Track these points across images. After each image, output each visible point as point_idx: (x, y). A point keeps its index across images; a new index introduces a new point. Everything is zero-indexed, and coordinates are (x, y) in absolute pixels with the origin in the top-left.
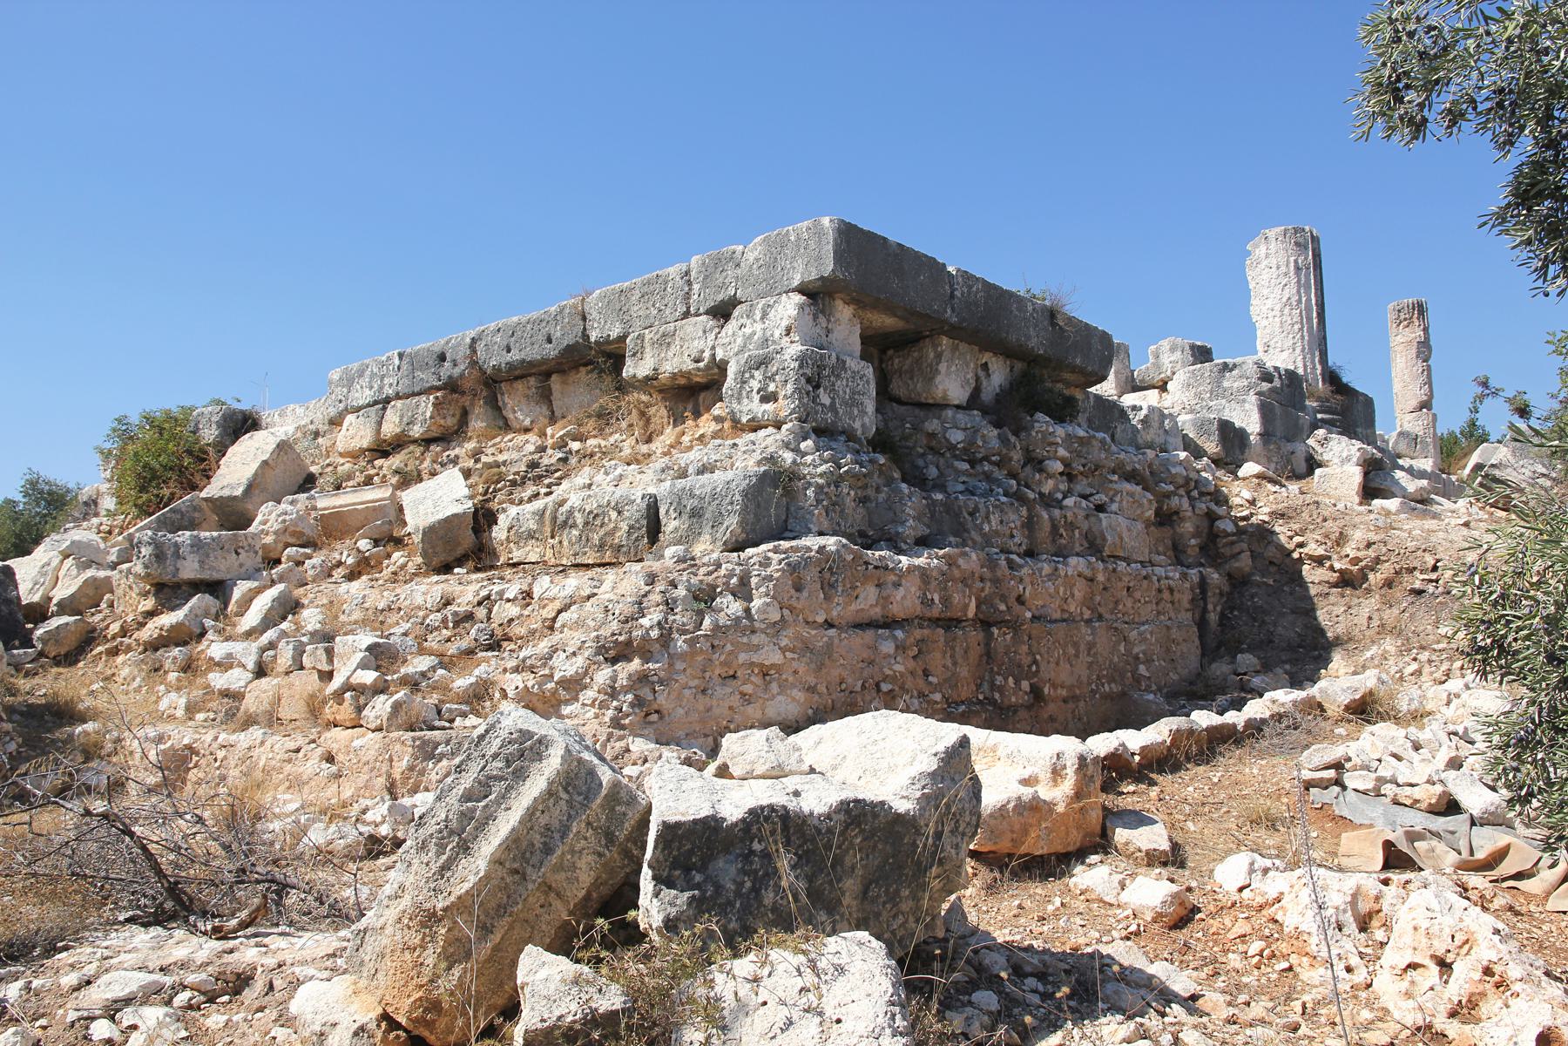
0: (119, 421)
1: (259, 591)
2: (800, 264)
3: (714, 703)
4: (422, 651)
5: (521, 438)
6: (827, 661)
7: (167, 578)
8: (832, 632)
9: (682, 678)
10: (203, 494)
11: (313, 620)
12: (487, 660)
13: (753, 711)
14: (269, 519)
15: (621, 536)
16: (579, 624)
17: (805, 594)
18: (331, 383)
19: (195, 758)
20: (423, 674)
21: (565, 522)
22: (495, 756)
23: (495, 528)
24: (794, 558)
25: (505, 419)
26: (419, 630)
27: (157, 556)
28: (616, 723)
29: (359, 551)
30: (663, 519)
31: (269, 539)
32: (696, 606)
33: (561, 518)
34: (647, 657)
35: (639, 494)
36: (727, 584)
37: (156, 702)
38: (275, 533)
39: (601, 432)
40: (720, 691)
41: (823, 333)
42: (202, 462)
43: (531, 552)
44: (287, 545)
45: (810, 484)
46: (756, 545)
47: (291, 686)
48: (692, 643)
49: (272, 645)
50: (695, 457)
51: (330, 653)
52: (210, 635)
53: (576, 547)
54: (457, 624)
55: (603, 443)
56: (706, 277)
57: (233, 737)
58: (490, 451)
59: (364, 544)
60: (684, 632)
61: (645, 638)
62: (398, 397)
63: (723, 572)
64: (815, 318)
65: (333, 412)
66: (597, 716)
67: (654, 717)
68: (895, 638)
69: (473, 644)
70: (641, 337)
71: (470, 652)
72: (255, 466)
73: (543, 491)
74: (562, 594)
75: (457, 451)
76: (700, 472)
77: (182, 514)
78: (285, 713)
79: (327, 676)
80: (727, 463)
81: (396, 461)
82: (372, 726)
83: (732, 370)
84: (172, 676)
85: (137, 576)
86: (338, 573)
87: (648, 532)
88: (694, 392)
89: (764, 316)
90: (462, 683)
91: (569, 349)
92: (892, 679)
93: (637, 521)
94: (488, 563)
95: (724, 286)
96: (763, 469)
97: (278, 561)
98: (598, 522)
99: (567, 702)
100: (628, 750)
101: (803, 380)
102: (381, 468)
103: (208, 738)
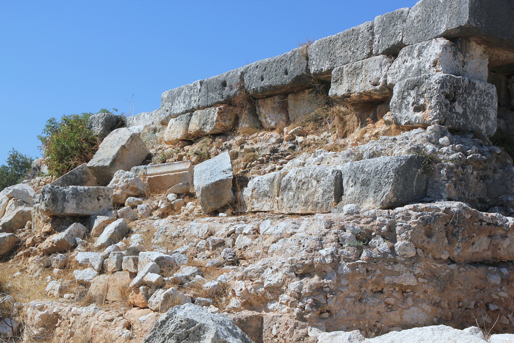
0: (50, 121)
1: (109, 222)
2: (445, 19)
3: (367, 308)
4: (191, 263)
5: (269, 134)
6: (449, 286)
7: (58, 213)
8: (453, 266)
9: (345, 291)
10: (88, 165)
11: (136, 241)
12: (228, 272)
13: (394, 317)
14: (120, 179)
15: (318, 197)
16: (282, 251)
17: (434, 239)
18: (162, 100)
19: (59, 321)
20: (187, 278)
21: (286, 187)
22: (171, 335)
23: (245, 189)
24: (427, 215)
25: (261, 122)
26: (192, 251)
27: (53, 200)
28: (300, 317)
29: (168, 200)
30: (345, 187)
31: (118, 192)
32: (356, 243)
33: (283, 184)
34: (323, 275)
35: (331, 170)
36: (379, 230)
37: (46, 286)
38: (122, 188)
39: (316, 131)
40: (371, 301)
41: (460, 65)
42: (92, 145)
43: (265, 205)
44: (128, 196)
45: (443, 166)
46: (402, 205)
47: (114, 280)
48: (353, 267)
49: (106, 257)
50: (367, 147)
51: (136, 261)
52: (79, 248)
53: (291, 203)
54: (214, 247)
55: (316, 138)
56: (383, 30)
57: (79, 310)
58: (249, 142)
59: (171, 196)
60: (348, 260)
61: (322, 263)
62: (199, 108)
63: (377, 222)
64: (455, 54)
65: (163, 117)
66: (289, 311)
67: (326, 315)
68: (501, 273)
69: (222, 261)
70: (341, 70)
71: (219, 265)
72: (117, 148)
73: (278, 167)
74: (276, 232)
75: (231, 142)
76: (371, 157)
77: (76, 176)
78: (111, 296)
79: (133, 275)
80: (389, 151)
81: (196, 147)
82: (154, 308)
83: (396, 90)
84: (56, 271)
85: (42, 210)
86: (156, 213)
87: (335, 195)
88: (373, 105)
89: (420, 54)
90: (209, 284)
91: (298, 79)
92: (499, 302)
93: (328, 187)
94: (240, 210)
95: (395, 35)
96: (410, 155)
97: (123, 205)
98: (305, 187)
99: (272, 301)
100: (307, 335)
101: (443, 96)
102: (188, 151)
103: (67, 309)
